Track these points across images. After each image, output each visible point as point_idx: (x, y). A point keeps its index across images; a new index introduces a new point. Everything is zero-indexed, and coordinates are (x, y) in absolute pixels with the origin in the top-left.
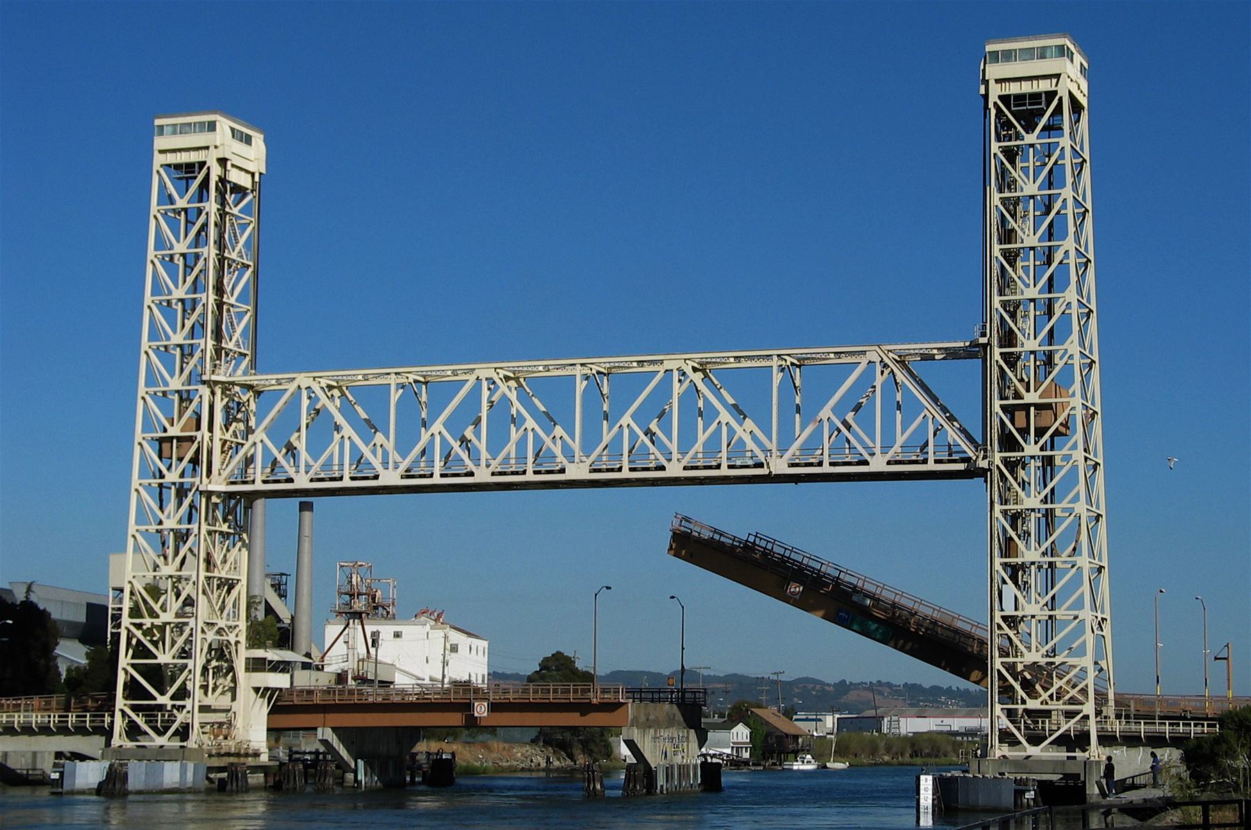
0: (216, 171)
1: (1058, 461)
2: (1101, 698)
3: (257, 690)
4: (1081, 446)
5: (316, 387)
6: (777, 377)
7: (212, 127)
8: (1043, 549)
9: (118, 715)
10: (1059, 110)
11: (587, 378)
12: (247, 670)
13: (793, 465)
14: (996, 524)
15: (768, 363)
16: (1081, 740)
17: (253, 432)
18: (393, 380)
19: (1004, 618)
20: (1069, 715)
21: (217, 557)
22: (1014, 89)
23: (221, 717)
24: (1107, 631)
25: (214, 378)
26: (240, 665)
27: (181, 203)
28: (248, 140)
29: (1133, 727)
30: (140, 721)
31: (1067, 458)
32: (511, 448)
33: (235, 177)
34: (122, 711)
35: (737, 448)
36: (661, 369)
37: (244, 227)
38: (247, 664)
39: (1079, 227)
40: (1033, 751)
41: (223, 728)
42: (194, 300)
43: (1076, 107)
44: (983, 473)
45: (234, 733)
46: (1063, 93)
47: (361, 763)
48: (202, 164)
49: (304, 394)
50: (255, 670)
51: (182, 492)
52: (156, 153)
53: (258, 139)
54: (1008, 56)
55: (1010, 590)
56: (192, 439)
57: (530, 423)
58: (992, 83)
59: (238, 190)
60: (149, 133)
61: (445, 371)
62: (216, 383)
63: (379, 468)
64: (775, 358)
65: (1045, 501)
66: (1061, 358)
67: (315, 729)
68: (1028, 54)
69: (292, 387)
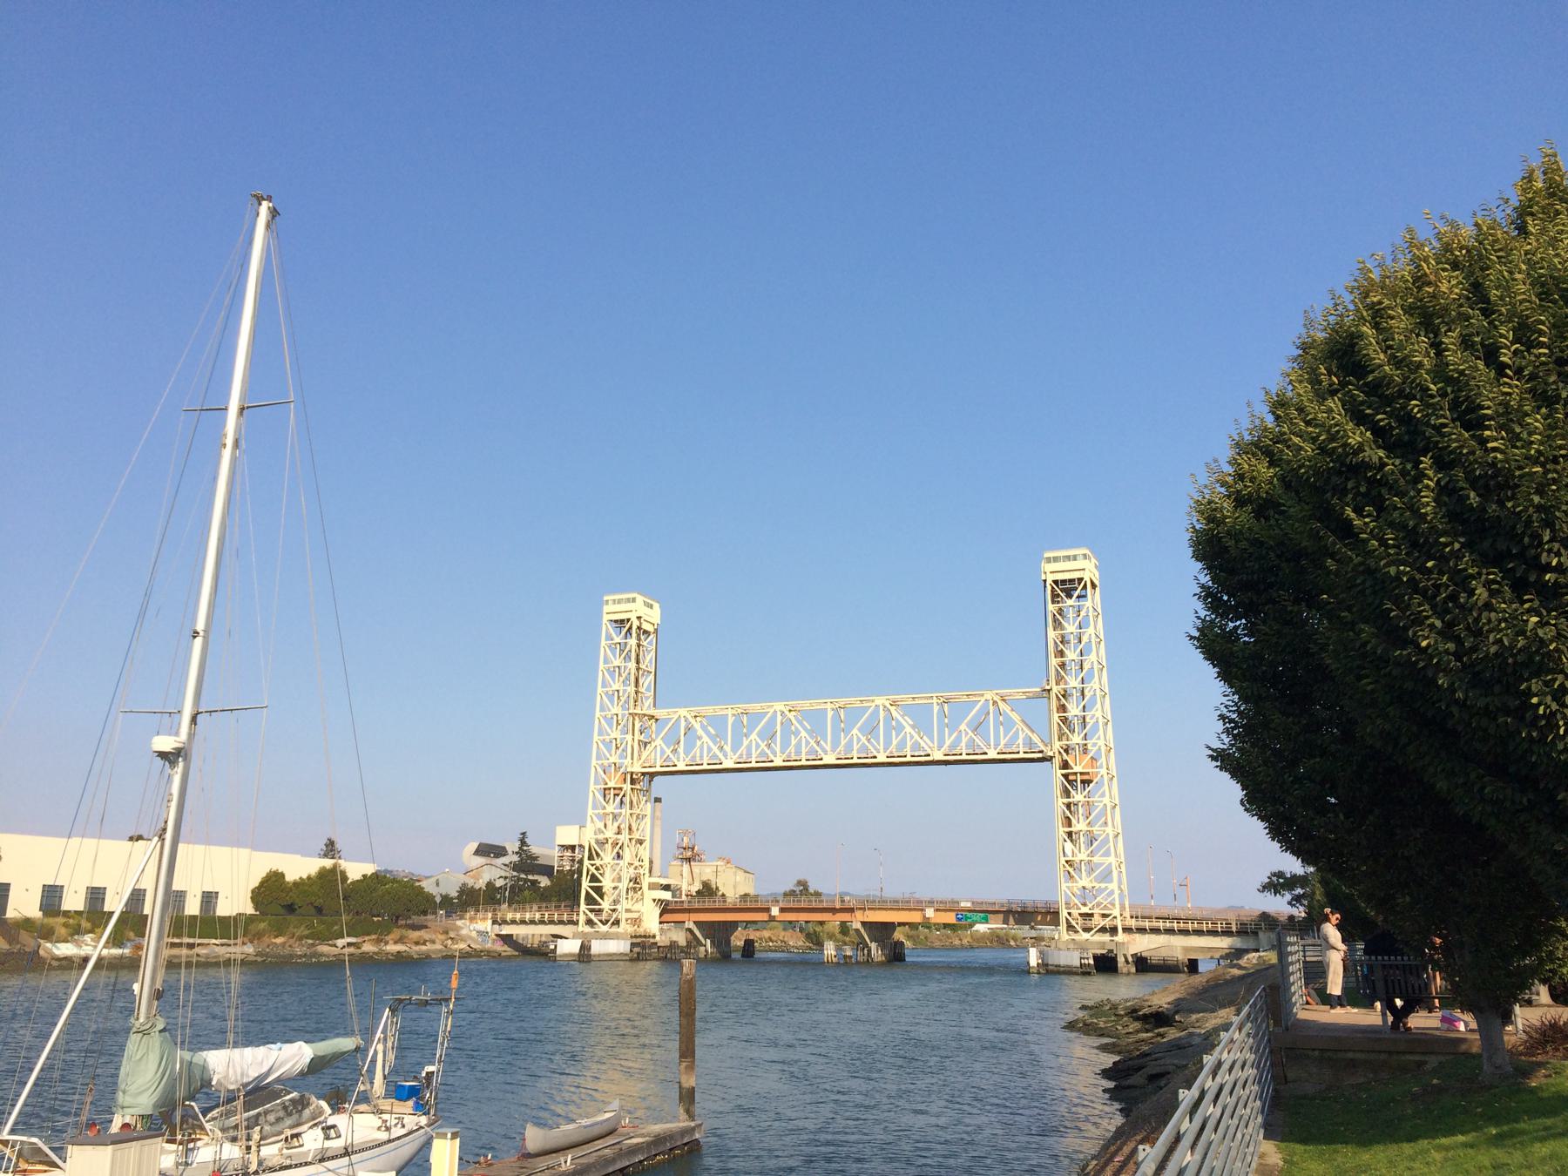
0: (636, 623)
1: (1089, 747)
2: (1123, 907)
3: (654, 900)
4: (1105, 767)
5: (689, 717)
6: (936, 708)
7: (634, 600)
8: (1084, 794)
9: (581, 913)
10: (1085, 587)
11: (833, 709)
12: (649, 889)
13: (945, 755)
14: (1059, 808)
15: (930, 701)
16: (1113, 930)
17: (654, 741)
18: (730, 712)
19: (1067, 862)
20: (1104, 916)
21: (634, 827)
22: (1060, 577)
23: (635, 915)
24: (1123, 869)
25: (635, 711)
26: (645, 886)
27: (617, 640)
28: (651, 606)
29: (1141, 923)
30: (592, 916)
31: (1094, 745)
32: (792, 749)
33: (645, 626)
34: (584, 912)
35: (916, 746)
36: (873, 705)
37: (649, 652)
38: (649, 886)
39: (1096, 622)
40: (1086, 936)
41: (636, 922)
42: (626, 643)
43: (1094, 586)
44: (1050, 759)
45: (642, 924)
46: (1087, 579)
47: (708, 941)
48: (628, 620)
49: (683, 720)
50: (653, 889)
51: (615, 817)
52: (605, 615)
53: (656, 606)
54: (1056, 559)
55: (1069, 846)
56: (621, 789)
57: (803, 734)
58: (1048, 573)
59: (646, 632)
60: (602, 603)
61: (755, 707)
62: (636, 714)
63: (723, 759)
64: (935, 698)
65: (1088, 855)
66: (1089, 691)
67: (684, 922)
68: (1068, 558)
69: (676, 717)
